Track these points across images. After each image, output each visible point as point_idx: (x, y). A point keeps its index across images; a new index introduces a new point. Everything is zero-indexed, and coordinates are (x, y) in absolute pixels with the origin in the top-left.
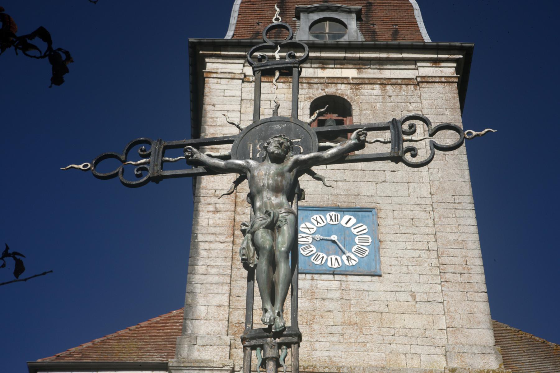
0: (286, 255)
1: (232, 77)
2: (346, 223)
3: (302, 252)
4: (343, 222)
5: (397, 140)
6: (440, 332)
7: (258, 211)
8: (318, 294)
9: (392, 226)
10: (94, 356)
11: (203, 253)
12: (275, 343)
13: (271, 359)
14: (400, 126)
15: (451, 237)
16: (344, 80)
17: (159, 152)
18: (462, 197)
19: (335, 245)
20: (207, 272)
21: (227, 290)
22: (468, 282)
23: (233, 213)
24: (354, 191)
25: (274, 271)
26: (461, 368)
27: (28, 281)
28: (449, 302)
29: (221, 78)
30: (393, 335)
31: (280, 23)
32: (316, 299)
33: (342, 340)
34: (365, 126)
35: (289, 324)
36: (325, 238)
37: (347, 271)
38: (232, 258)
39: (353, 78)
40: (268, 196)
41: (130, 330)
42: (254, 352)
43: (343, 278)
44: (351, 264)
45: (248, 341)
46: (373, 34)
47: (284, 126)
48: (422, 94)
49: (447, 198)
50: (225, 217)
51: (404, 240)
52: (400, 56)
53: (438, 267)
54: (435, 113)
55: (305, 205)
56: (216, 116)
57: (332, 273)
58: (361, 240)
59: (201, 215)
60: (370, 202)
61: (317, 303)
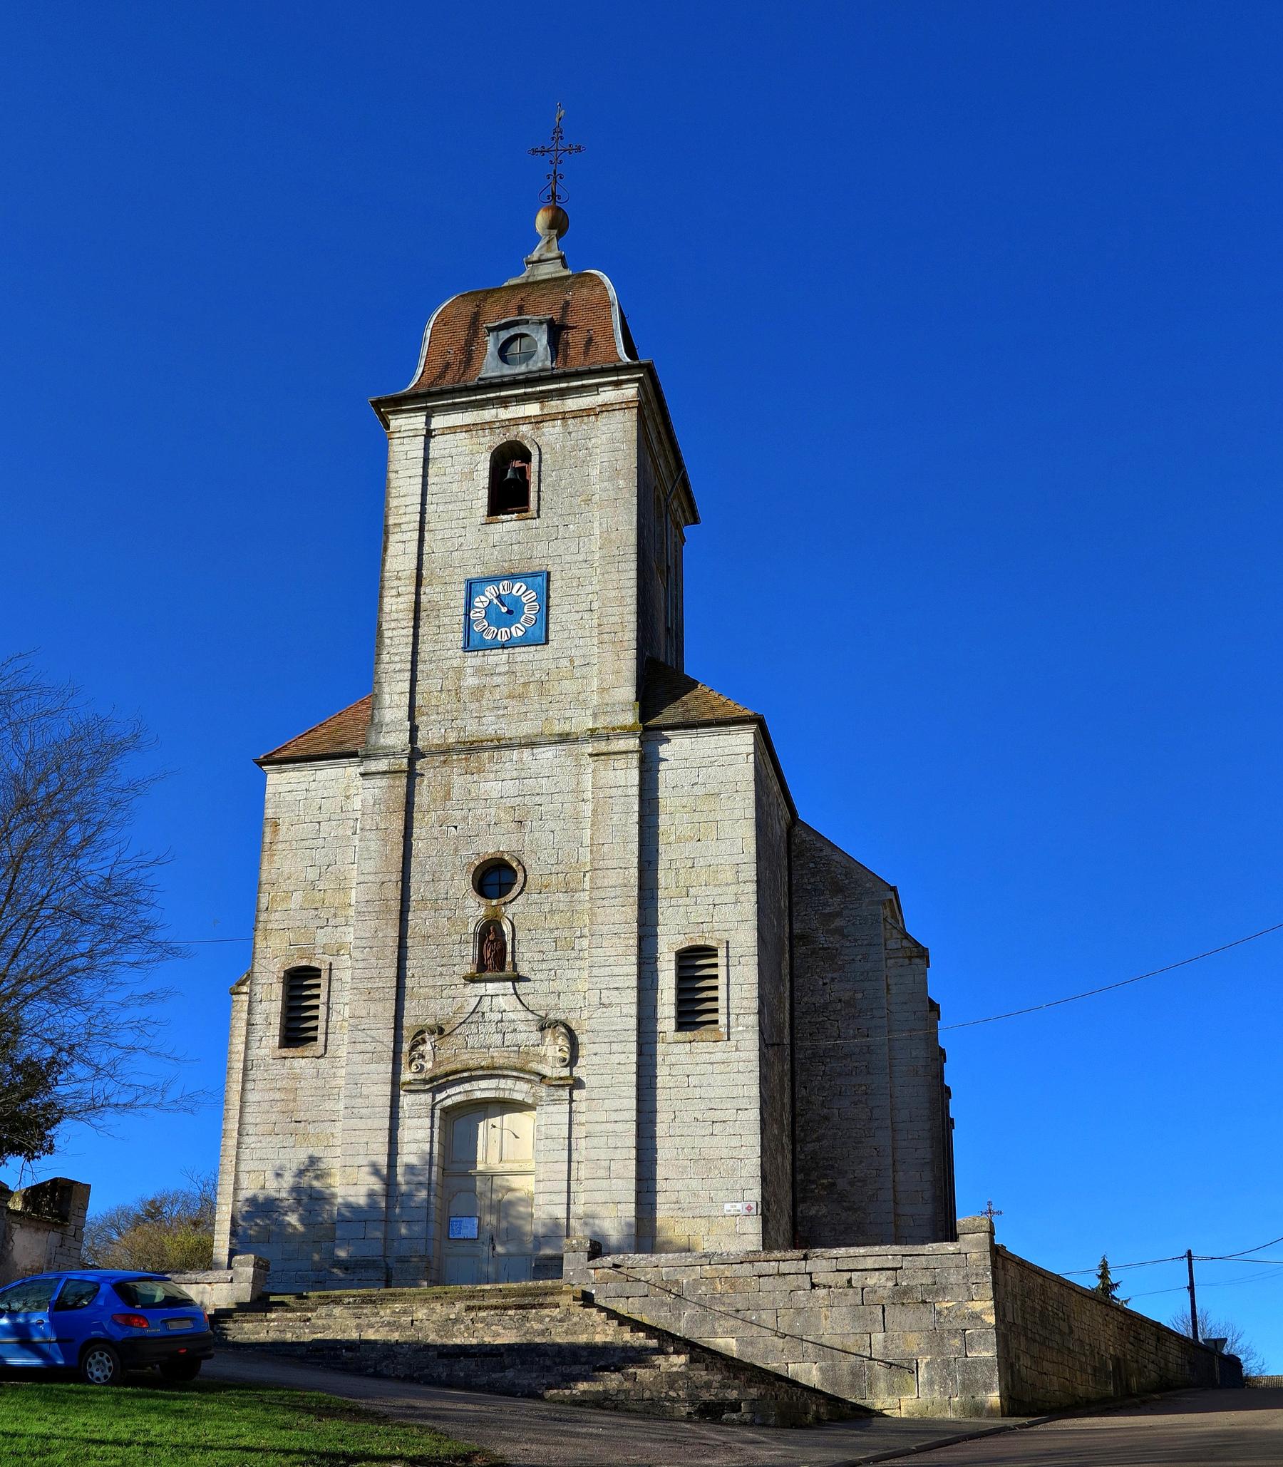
11: (387, 641)
16: (526, 420)
52: (580, 383)
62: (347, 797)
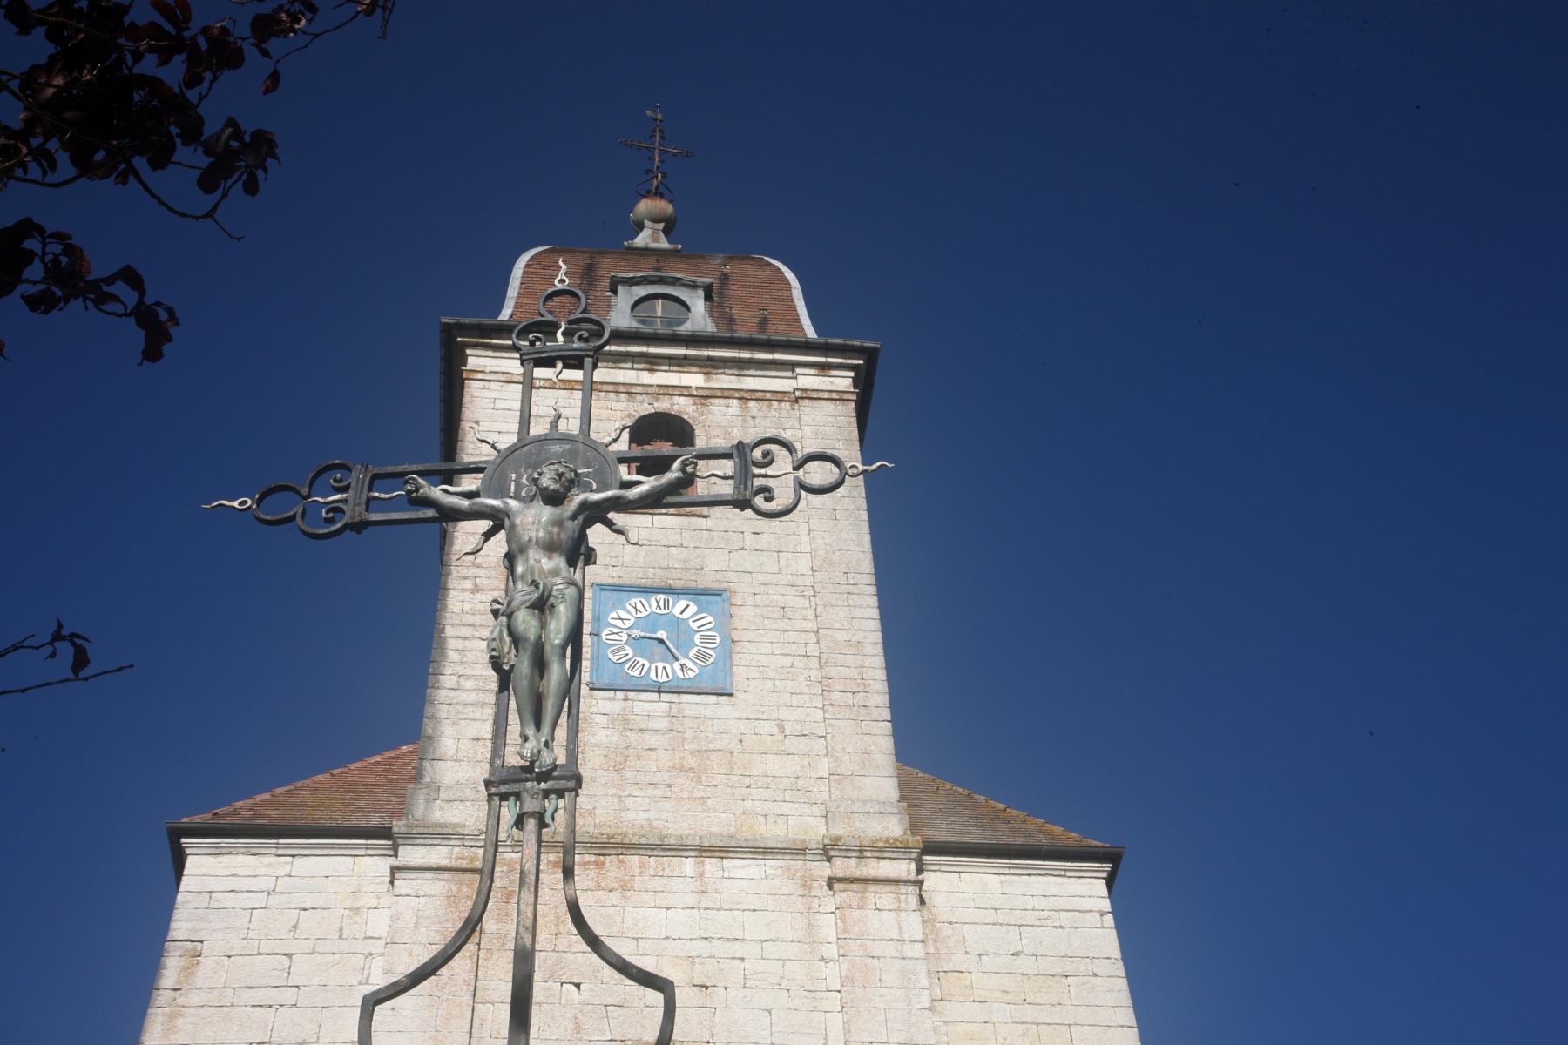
0: (561, 651)
1: (508, 379)
2: (682, 613)
3: (610, 656)
4: (677, 611)
5: (743, 474)
6: (819, 781)
9: (751, 619)
11: (453, 655)
12: (539, 789)
13: (532, 814)
14: (749, 453)
15: (841, 636)
16: (683, 391)
17: (363, 484)
21: (489, 715)
22: (864, 706)
24: (695, 562)
25: (541, 677)
27: (90, 680)
28: (834, 736)
29: (490, 381)
30: (747, 787)
32: (631, 730)
33: (669, 794)
35: (562, 760)
36: (648, 635)
37: (681, 687)
39: (697, 388)
40: (536, 557)
41: (332, 775)
43: (674, 698)
44: (687, 677)
46: (730, 322)
47: (567, 447)
49: (837, 576)
53: (820, 682)
55: (618, 583)
57: (656, 689)
58: (704, 640)
59: (451, 596)
60: (719, 581)
61: (633, 737)
62: (356, 911)
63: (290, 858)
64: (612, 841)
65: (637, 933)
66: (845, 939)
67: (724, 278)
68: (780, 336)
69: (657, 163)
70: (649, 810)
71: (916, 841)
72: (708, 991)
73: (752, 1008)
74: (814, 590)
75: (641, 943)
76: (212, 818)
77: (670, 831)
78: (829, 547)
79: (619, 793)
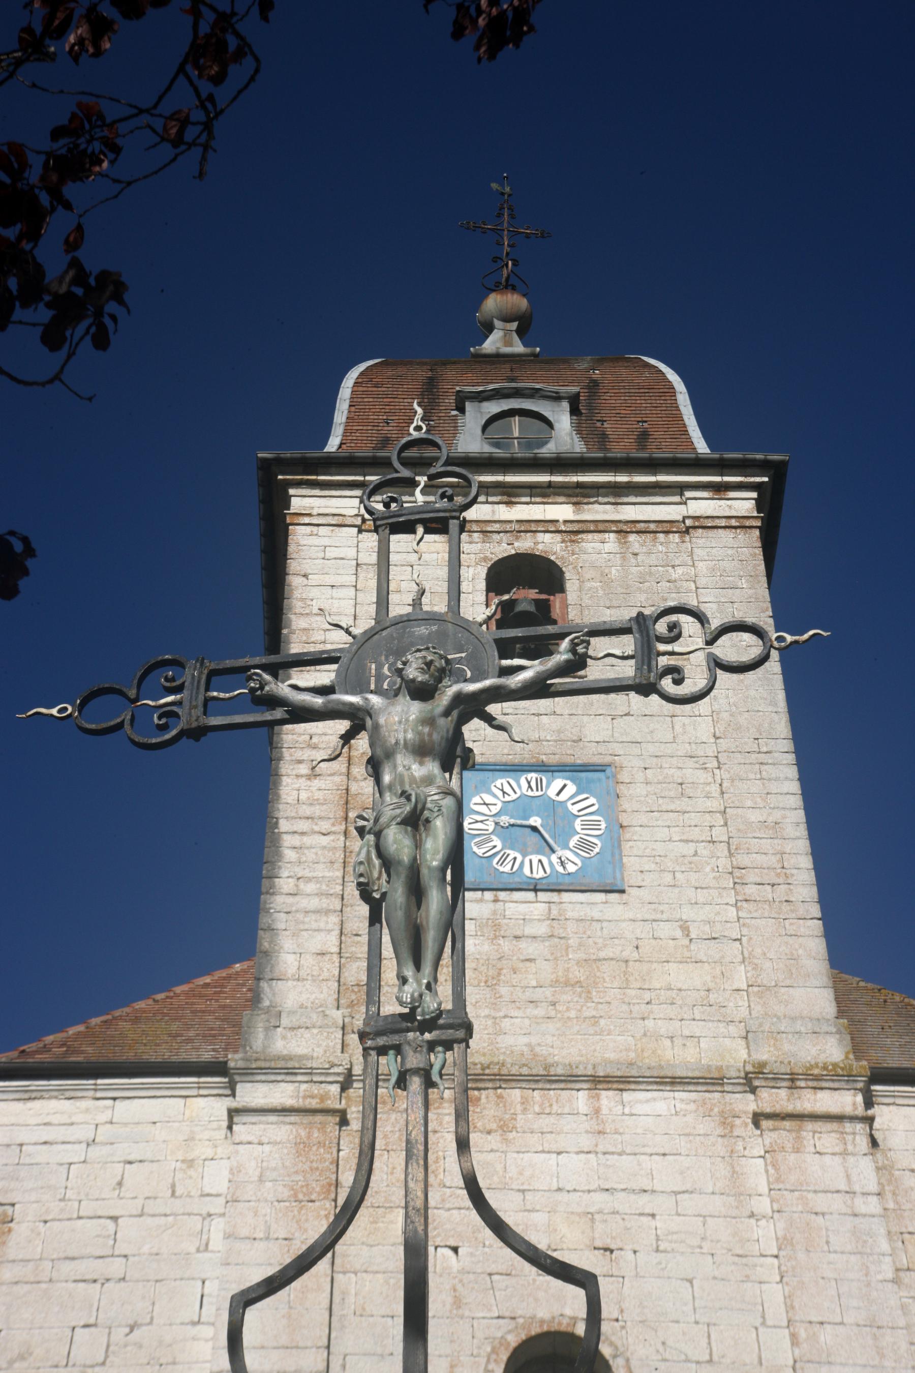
0: (441, 875)
2: (558, 794)
3: (475, 849)
4: (552, 792)
5: (646, 653)
6: (736, 994)
7: (387, 790)
8: (506, 927)
9: (643, 799)
10: (90, 1049)
11: (289, 855)
12: (423, 1041)
13: (416, 1071)
14: (651, 627)
15: (754, 816)
16: (549, 526)
17: (199, 682)
18: (772, 742)
19: (536, 834)
20: (298, 890)
21: (335, 924)
22: (786, 901)
23: (345, 778)
25: (419, 906)
26: (776, 1062)
28: (751, 938)
30: (648, 1003)
31: (425, 436)
33: (553, 1014)
34: (586, 626)
35: (448, 1005)
36: (519, 822)
37: (560, 884)
38: (344, 862)
39: (565, 522)
41: (154, 1000)
42: (383, 1060)
43: (554, 897)
45: (372, 1039)
46: (602, 439)
47: (434, 628)
48: (695, 550)
49: (746, 743)
50: (330, 786)
51: (667, 824)
52: (652, 479)
53: (731, 873)
54: (720, 584)
56: (311, 595)
57: (532, 887)
58: (586, 826)
59: (284, 783)
60: (601, 754)
61: (506, 946)
62: (190, 1163)
63: (110, 1102)
64: (487, 1071)
65: (523, 1184)
66: (779, 1190)
67: (593, 386)
68: (664, 452)
69: (506, 248)
70: (529, 1034)
71: (861, 1067)
72: (614, 1256)
73: (669, 1278)
74: (719, 762)
75: (529, 1196)
76: (19, 1057)
77: (556, 1058)
78: (734, 709)
79: (493, 1013)
